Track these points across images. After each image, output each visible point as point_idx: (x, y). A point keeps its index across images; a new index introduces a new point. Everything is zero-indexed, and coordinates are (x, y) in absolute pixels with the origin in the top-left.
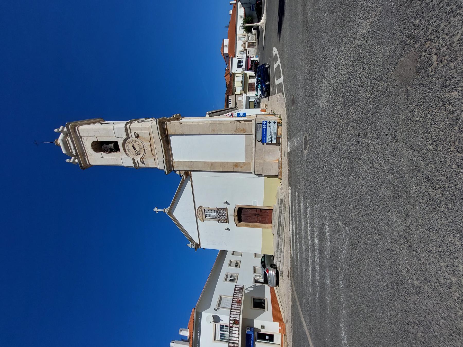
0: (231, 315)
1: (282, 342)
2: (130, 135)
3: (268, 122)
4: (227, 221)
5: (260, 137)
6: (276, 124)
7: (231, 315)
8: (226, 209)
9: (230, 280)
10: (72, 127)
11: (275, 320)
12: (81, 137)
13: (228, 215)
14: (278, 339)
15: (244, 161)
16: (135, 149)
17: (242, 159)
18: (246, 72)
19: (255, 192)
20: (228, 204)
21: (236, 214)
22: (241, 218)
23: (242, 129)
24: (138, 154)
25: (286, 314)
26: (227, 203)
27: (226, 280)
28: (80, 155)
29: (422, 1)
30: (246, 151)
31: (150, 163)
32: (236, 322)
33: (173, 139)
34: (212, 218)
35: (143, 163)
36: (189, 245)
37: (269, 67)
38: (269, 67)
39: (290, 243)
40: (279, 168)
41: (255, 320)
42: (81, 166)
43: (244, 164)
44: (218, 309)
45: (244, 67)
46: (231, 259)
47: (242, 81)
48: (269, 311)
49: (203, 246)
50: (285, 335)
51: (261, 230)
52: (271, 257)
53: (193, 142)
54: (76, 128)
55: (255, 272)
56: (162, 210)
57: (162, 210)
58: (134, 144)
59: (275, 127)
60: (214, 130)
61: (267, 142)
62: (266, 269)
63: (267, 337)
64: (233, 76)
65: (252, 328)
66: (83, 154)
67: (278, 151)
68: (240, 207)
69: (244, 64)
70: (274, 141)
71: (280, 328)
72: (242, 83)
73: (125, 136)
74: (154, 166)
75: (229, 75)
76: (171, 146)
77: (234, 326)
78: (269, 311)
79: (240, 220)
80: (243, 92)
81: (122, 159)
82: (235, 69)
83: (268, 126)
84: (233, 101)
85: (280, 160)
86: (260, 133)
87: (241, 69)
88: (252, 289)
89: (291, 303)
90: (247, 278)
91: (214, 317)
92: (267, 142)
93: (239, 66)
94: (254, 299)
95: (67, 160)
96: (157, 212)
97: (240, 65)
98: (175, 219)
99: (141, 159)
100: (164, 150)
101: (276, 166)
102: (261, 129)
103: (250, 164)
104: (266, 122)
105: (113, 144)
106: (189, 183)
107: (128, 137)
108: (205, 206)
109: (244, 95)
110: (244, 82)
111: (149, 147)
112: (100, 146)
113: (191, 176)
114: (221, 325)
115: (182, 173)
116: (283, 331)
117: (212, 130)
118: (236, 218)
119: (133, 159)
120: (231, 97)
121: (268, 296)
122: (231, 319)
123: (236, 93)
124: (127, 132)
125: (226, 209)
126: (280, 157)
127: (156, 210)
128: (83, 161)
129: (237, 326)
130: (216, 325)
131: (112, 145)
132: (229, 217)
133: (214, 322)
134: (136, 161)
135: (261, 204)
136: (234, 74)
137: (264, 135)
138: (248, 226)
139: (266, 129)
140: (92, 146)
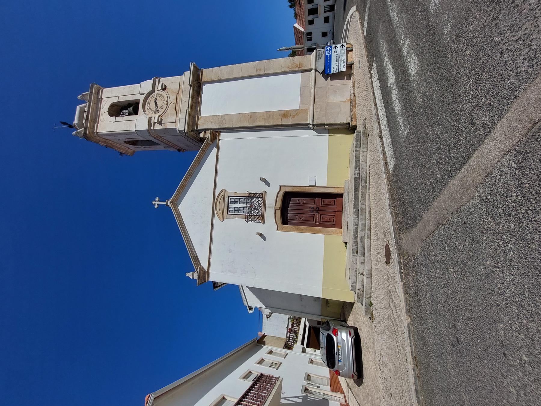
4: (261, 219)
5: (321, 68)
6: (344, 48)
8: (263, 196)
15: (298, 108)
16: (156, 105)
17: (296, 106)
20: (267, 183)
21: (279, 204)
26: (263, 180)
28: (91, 120)
29: (499, 3)
30: (301, 95)
33: (207, 89)
35: (160, 123)
36: (190, 275)
40: (351, 109)
43: (297, 112)
49: (212, 278)
51: (323, 236)
56: (165, 203)
57: (165, 203)
58: (158, 98)
61: (332, 72)
66: (95, 120)
70: (343, 68)
73: (150, 89)
81: (138, 123)
83: (333, 52)
99: (159, 117)
100: (192, 101)
101: (347, 108)
102: (323, 57)
103: (306, 111)
106: (215, 150)
107: (153, 91)
112: (117, 110)
113: (219, 140)
115: (208, 135)
118: (279, 213)
125: (263, 196)
128: (90, 128)
132: (267, 210)
134: (152, 121)
138: (299, 230)
139: (331, 56)
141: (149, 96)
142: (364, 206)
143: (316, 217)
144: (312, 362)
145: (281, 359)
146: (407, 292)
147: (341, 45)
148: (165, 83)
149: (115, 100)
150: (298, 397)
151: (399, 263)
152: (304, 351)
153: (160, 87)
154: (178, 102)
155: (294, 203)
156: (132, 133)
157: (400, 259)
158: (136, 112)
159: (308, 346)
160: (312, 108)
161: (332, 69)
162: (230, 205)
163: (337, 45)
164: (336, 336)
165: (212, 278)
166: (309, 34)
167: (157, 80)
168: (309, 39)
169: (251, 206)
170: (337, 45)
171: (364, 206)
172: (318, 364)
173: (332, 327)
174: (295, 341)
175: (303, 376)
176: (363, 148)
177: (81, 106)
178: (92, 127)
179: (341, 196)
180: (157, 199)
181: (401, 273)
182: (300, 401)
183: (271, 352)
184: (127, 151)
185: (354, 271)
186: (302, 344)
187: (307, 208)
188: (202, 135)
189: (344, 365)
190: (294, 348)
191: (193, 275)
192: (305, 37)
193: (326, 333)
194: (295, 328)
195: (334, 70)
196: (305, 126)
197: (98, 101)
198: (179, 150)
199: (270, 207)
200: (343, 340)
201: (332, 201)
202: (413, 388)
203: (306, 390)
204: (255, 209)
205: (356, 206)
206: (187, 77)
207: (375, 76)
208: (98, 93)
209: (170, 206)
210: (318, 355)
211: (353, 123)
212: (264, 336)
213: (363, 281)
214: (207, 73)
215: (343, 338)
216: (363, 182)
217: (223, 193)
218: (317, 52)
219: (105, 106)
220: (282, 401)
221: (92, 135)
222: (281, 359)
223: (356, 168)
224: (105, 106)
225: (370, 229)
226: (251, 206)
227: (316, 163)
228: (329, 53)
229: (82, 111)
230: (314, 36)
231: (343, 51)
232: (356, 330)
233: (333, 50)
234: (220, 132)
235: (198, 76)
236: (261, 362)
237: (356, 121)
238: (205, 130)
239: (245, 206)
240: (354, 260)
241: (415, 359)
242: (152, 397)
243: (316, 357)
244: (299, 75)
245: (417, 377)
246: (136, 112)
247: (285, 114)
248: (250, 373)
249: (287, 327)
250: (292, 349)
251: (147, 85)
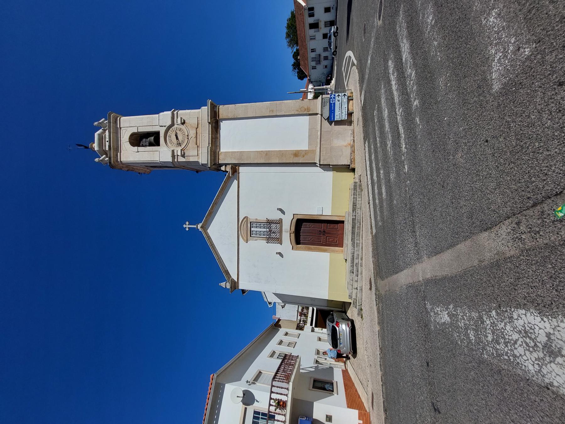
0: (274, 389)
4: (279, 241)
5: (326, 114)
6: (346, 97)
7: (274, 389)
8: (280, 222)
16: (177, 138)
17: (304, 146)
20: (283, 212)
23: (306, 107)
24: (179, 144)
26: (281, 210)
28: (113, 149)
30: (310, 136)
33: (224, 125)
35: (183, 156)
36: (223, 284)
39: (371, 222)
40: (351, 153)
41: (315, 404)
43: (306, 152)
44: (254, 383)
46: (282, 339)
49: (241, 287)
53: (245, 133)
56: (195, 226)
57: (195, 226)
58: (178, 132)
59: (345, 100)
61: (336, 119)
62: (335, 323)
66: (117, 148)
67: (350, 132)
68: (299, 217)
70: (345, 117)
71: (361, 422)
73: (169, 123)
76: (220, 134)
79: (298, 241)
81: (161, 154)
83: (336, 100)
86: (327, 108)
89: (377, 328)
92: (336, 119)
96: (187, 229)
99: (181, 150)
100: (212, 137)
102: (328, 104)
103: (313, 152)
105: (153, 138)
106: (235, 182)
107: (173, 124)
112: (138, 139)
113: (239, 173)
114: (255, 412)
115: (229, 169)
117: (270, 111)
118: (293, 236)
119: (173, 151)
122: (274, 396)
125: (280, 222)
130: (246, 409)
131: (152, 138)
132: (284, 233)
133: (244, 404)
134: (176, 154)
137: (332, 111)
139: (334, 104)
141: (169, 129)
142: (358, 241)
143: (323, 238)
144: (320, 339)
145: (295, 339)
146: (378, 312)
147: (343, 94)
148: (184, 118)
149: (135, 130)
151: (376, 294)
152: (313, 331)
153: (179, 122)
154: (198, 136)
155: (304, 228)
156: (158, 163)
157: (376, 292)
158: (157, 143)
159: (316, 326)
161: (336, 117)
162: (252, 229)
163: (340, 94)
164: (338, 327)
165: (241, 287)
166: (311, 9)
167: (175, 113)
168: (311, 15)
169: (271, 231)
170: (340, 94)
171: (358, 241)
172: (324, 341)
173: (335, 320)
174: (305, 322)
175: (314, 352)
176: (359, 198)
177: (98, 132)
178: (115, 156)
179: (343, 222)
180: (187, 223)
181: (376, 301)
182: (314, 370)
183: (286, 334)
184: (146, 171)
185: (351, 284)
186: (311, 324)
187: (314, 232)
188: (223, 168)
189: (344, 346)
190: (305, 329)
191: (226, 285)
192: (306, 13)
193: (331, 325)
194: (305, 310)
195: (337, 118)
196: (314, 164)
197: (116, 131)
198: (197, 172)
199: (285, 231)
200: (343, 330)
201: (336, 226)
202: (379, 363)
203: (317, 362)
204: (273, 233)
205: (353, 233)
206: (204, 112)
207: (367, 149)
208: (116, 122)
209: (200, 230)
210: (324, 333)
211: (352, 166)
212: (279, 320)
213: (357, 293)
214: (224, 110)
215: (344, 328)
216: (358, 223)
217: (245, 219)
218: (322, 99)
219: (125, 137)
220: (301, 371)
221: (117, 163)
222: (295, 339)
223: (353, 211)
224: (125, 137)
225: (362, 259)
226: (270, 231)
227: (322, 195)
229: (101, 138)
230: (316, 12)
231: (345, 100)
232: (352, 322)
233: (337, 98)
234: (239, 166)
235: (215, 113)
236: (281, 343)
237: (355, 164)
238: (226, 165)
239: (265, 230)
240: (351, 278)
241: (380, 349)
242: (215, 376)
243: (323, 335)
244: (307, 118)
245: (381, 358)
246: (157, 143)
247: (296, 154)
248: (274, 352)
249: (298, 311)
250: (303, 330)
251: (165, 117)
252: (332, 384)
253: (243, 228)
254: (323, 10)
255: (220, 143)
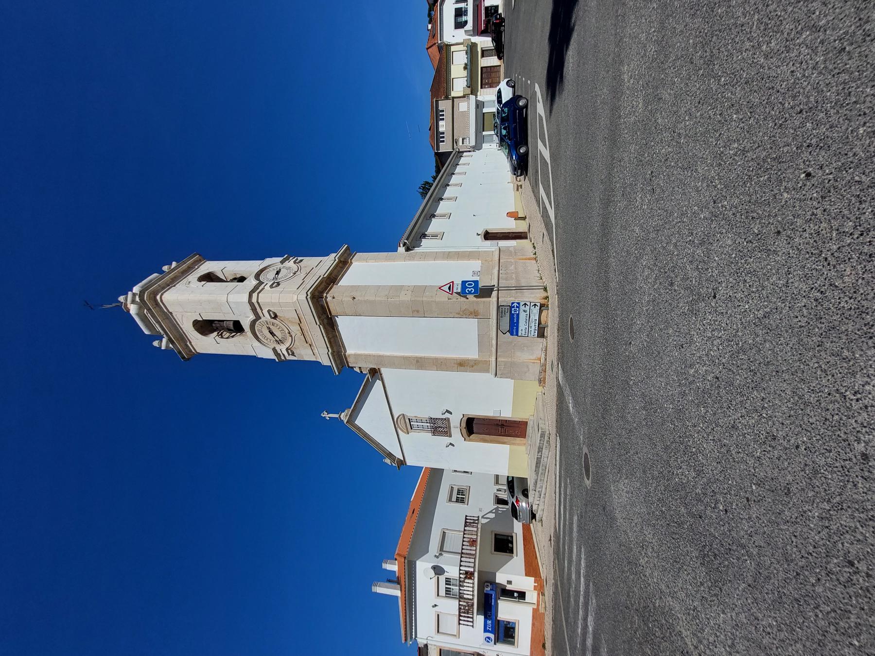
1: (538, 601)
2: (261, 315)
3: (522, 304)
4: (447, 433)
9: (457, 501)
10: (149, 298)
11: (528, 574)
12: (171, 313)
13: (450, 427)
14: (532, 596)
18: (476, 39)
19: (497, 399)
21: (464, 425)
22: (472, 428)
24: (280, 342)
25: (546, 569)
26: (448, 411)
27: (450, 500)
28: (177, 340)
31: (304, 354)
32: (469, 575)
33: (343, 323)
34: (423, 429)
35: (293, 354)
36: (388, 461)
37: (526, 106)
38: (526, 106)
42: (184, 358)
44: (441, 554)
45: (469, 26)
47: (466, 64)
48: (518, 559)
50: (543, 594)
51: (506, 447)
52: (523, 481)
54: (158, 297)
55: (497, 482)
58: (271, 327)
60: (418, 312)
63: (516, 595)
64: (445, 50)
65: (493, 583)
66: (182, 338)
69: (470, 18)
72: (465, 68)
74: (313, 359)
75: (435, 48)
76: (339, 332)
77: (467, 581)
78: (518, 559)
80: (469, 91)
82: (451, 34)
83: (521, 311)
84: (447, 114)
85: (543, 361)
87: (461, 31)
88: (492, 516)
90: (482, 504)
91: (435, 568)
93: (459, 25)
94: (496, 535)
95: (156, 344)
97: (459, 20)
98: (359, 429)
100: (328, 338)
104: (519, 303)
108: (410, 414)
109: (472, 97)
110: (471, 66)
111: (299, 333)
116: (540, 588)
118: (464, 431)
119: (274, 350)
120: (444, 105)
121: (518, 528)
123: (453, 94)
124: (254, 310)
126: (543, 356)
127: (325, 415)
128: (183, 349)
129: (471, 581)
134: (279, 352)
135: (507, 414)
136: (448, 46)
139: (518, 315)
140: (196, 330)
150: (491, 512)
160: (494, 359)
208: (157, 304)
228: (515, 311)
235: (323, 307)
252: (512, 537)
253: (401, 424)
254: (481, 231)
255: (342, 342)
